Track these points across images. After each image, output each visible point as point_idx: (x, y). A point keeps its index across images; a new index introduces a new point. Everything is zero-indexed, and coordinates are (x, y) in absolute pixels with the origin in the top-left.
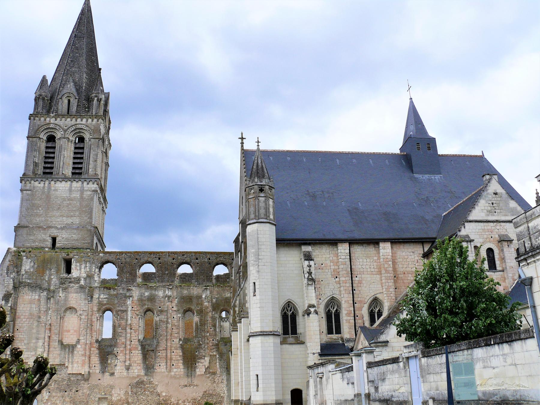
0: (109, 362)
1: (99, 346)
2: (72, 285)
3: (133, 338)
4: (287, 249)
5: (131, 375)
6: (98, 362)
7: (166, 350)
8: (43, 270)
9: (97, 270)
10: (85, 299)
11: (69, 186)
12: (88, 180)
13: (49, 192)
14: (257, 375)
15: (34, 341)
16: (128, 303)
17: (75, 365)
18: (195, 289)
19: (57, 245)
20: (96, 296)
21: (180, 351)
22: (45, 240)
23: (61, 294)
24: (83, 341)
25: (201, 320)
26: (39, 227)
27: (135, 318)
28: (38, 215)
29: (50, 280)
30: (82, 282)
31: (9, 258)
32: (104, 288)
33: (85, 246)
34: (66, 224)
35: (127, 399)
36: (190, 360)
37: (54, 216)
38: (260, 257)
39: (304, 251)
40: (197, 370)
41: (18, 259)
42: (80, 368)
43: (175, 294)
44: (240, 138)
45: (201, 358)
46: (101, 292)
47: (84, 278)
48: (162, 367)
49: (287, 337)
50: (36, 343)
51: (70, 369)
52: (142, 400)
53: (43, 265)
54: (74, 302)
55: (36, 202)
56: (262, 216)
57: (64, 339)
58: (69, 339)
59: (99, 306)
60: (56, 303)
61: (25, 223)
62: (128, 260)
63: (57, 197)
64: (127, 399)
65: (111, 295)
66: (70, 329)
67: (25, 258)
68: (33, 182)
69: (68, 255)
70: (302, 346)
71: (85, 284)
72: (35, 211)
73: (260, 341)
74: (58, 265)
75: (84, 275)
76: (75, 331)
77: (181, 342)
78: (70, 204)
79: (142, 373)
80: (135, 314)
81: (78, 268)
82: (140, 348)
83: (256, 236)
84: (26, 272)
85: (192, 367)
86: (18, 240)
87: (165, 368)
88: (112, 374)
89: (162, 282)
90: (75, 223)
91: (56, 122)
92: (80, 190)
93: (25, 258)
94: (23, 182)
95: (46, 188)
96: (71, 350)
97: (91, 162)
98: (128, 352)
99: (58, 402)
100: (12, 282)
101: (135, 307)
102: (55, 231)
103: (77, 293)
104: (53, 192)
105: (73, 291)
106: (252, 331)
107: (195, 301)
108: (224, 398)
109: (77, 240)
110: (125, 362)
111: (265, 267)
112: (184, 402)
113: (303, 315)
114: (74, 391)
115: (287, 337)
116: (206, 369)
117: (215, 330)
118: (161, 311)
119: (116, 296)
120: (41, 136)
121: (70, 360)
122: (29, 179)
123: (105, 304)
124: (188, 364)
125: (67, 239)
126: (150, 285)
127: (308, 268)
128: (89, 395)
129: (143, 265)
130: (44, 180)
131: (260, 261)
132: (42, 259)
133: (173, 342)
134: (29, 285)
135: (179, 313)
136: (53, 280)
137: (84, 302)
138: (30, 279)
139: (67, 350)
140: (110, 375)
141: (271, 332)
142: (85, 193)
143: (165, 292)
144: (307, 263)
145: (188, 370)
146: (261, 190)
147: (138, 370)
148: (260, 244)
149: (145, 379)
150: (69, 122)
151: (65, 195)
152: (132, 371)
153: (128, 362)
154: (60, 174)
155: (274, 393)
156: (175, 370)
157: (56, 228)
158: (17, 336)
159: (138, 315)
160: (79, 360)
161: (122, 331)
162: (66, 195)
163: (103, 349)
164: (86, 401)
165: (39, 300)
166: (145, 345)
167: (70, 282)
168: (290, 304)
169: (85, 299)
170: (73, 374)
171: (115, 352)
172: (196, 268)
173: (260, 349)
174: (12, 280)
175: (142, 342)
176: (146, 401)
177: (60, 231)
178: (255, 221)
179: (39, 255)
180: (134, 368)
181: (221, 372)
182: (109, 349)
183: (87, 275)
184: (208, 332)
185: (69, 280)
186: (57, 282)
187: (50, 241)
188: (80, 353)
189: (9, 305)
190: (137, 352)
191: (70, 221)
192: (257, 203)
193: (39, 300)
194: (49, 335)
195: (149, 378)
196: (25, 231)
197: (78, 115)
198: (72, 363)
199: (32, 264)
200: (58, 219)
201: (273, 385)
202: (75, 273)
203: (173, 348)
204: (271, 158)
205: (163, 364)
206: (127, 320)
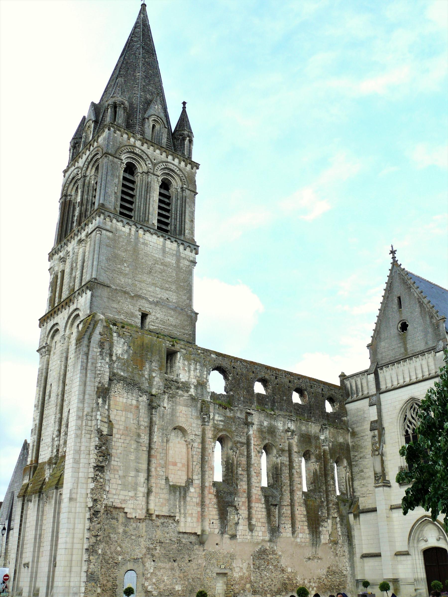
1: (217, 492)
6: (217, 517)
15: (132, 474)
17: (189, 519)
18: (313, 425)
21: (304, 509)
22: (132, 315)
26: (125, 292)
29: (151, 379)
30: (192, 391)
34: (160, 298)
40: (322, 537)
50: (136, 476)
51: (182, 524)
52: (265, 578)
54: (183, 419)
63: (147, 255)
64: (250, 576)
65: (228, 417)
66: (178, 461)
68: (114, 221)
69: (173, 345)
72: (119, 266)
75: (194, 381)
78: (164, 271)
81: (186, 368)
82: (263, 500)
85: (316, 532)
87: (291, 532)
88: (233, 537)
91: (143, 148)
92: (176, 255)
96: (182, 494)
99: (166, 578)
100: (108, 370)
103: (186, 406)
104: (142, 246)
105: (182, 402)
108: (347, 577)
109: (175, 326)
112: (310, 582)
121: (182, 511)
123: (221, 430)
134: (124, 379)
137: (195, 421)
138: (124, 371)
139: (178, 493)
145: (313, 535)
147: (261, 533)
149: (267, 546)
151: (157, 256)
157: (147, 299)
161: (243, 473)
165: (137, 407)
167: (178, 388)
171: (236, 504)
176: (270, 580)
177: (153, 306)
181: (343, 542)
183: (197, 381)
186: (161, 384)
187: (139, 315)
191: (165, 295)
193: (137, 407)
195: (272, 546)
199: (126, 348)
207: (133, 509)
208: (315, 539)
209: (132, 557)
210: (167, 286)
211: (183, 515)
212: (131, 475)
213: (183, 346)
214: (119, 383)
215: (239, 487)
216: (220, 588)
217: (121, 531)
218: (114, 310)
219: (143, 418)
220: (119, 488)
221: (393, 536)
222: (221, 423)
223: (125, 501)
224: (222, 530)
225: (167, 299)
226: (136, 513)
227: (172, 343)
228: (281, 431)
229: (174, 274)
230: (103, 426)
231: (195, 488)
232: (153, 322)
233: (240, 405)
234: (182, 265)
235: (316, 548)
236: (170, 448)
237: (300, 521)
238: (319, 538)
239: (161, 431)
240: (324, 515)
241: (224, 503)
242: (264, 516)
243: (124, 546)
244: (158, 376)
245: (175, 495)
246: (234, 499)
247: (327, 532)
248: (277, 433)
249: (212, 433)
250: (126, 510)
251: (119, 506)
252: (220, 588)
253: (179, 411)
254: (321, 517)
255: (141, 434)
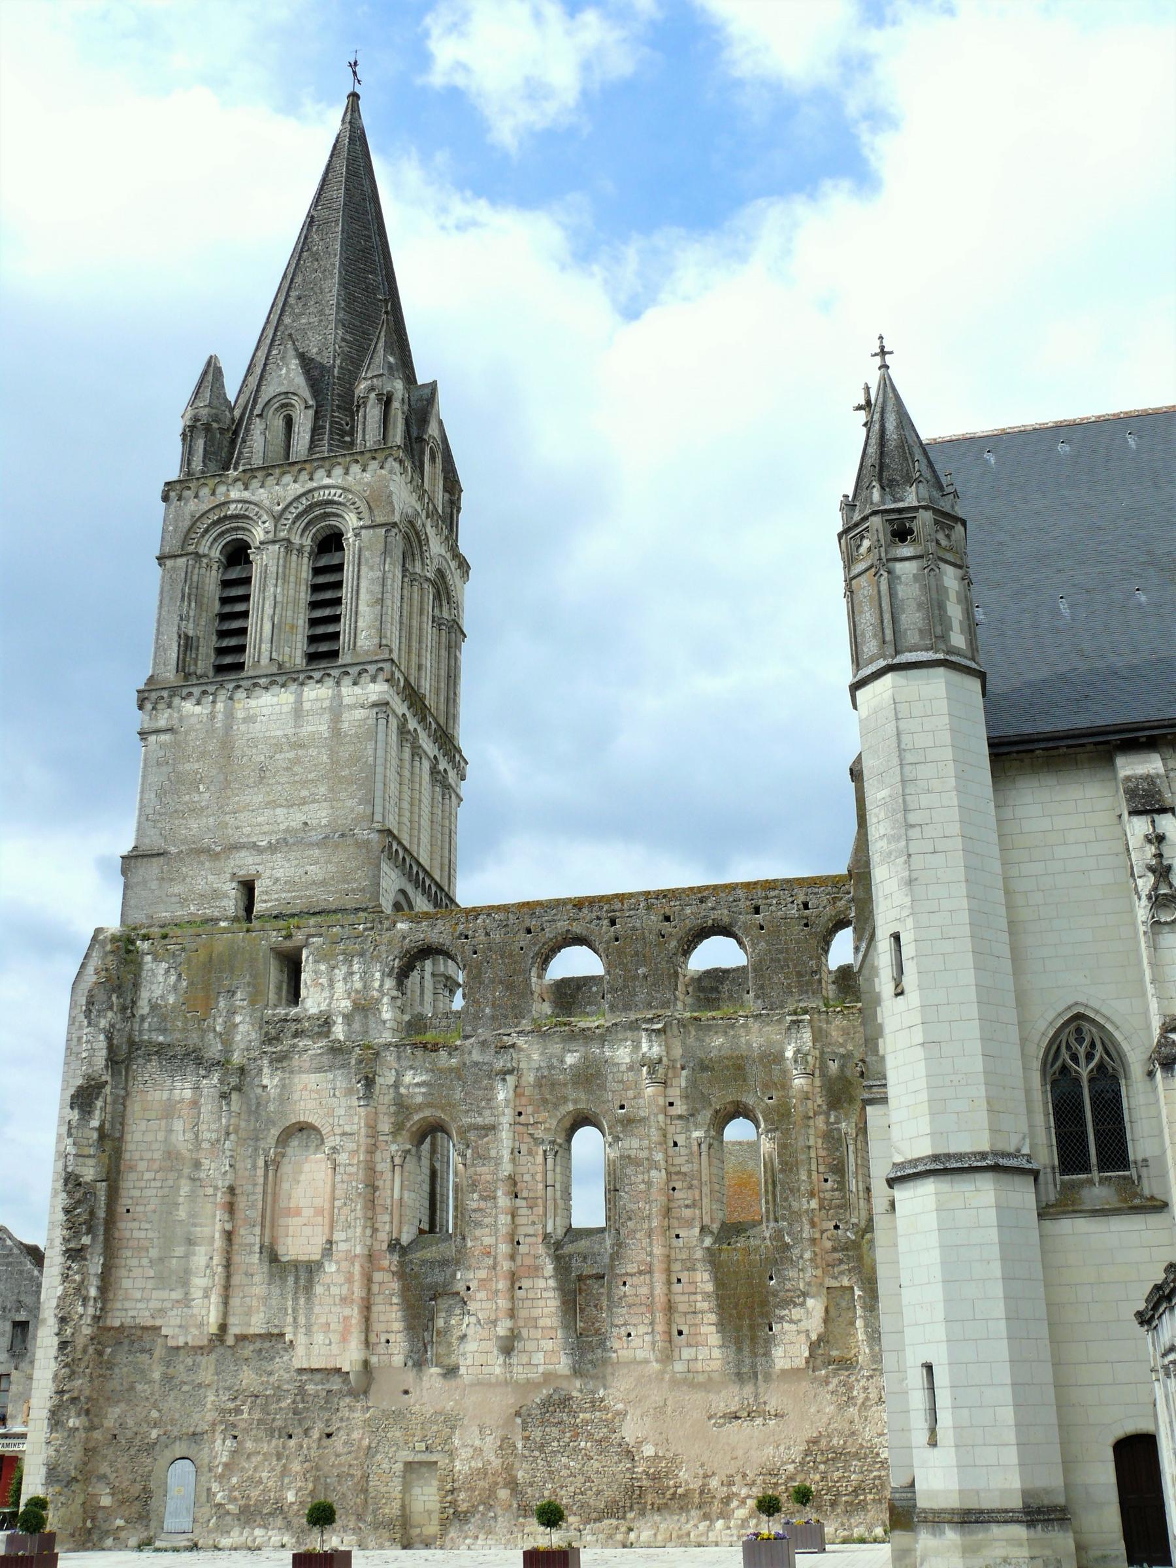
0: (440, 1323)
1: (402, 1264)
2: (302, 1043)
3: (522, 1230)
4: (1050, 780)
5: (520, 1374)
7: (650, 1272)
8: (208, 997)
9: (389, 983)
10: (349, 1092)
11: (292, 698)
12: (354, 671)
13: (228, 728)
14: (929, 1368)
16: (501, 1096)
17: (319, 1338)
19: (258, 907)
20: (386, 1078)
21: (706, 1276)
22: (216, 895)
23: (270, 1080)
24: (343, 1246)
25: (783, 1147)
27: (530, 1153)
28: (197, 811)
29: (231, 1028)
30: (339, 1031)
31: (95, 961)
32: (415, 1046)
33: (350, 902)
34: (287, 830)
35: (509, 1468)
36: (747, 1313)
37: (246, 808)
38: (913, 818)
39: (1128, 779)
40: (778, 1352)
41: (125, 963)
42: (335, 1349)
43: (678, 1052)
44: (859, 408)
45: (789, 1303)
46: (405, 1063)
47: (345, 1016)
48: (636, 1342)
49: (1082, 1183)
50: (187, 1256)
51: (300, 1350)
52: (564, 1472)
53: (208, 979)
54: (311, 1105)
55: (188, 766)
56: (913, 637)
57: (281, 1240)
58: (300, 1242)
59: (396, 1114)
60: (250, 1112)
61: (154, 841)
62: (497, 936)
63: (253, 742)
64: (509, 1468)
65: (441, 1071)
67: (148, 958)
69: (289, 937)
70: (1153, 1220)
71: (348, 1038)
73: (931, 1203)
74: (254, 976)
75: (345, 1005)
76: (319, 1212)
77: (708, 1241)
78: (297, 761)
79: (563, 1364)
80: (527, 1139)
82: (549, 1268)
83: (890, 729)
84: (154, 1007)
85: (753, 1339)
86: (132, 902)
87: (647, 1346)
88: (451, 1372)
89: (627, 1008)
90: (314, 822)
91: (246, 495)
92: (331, 708)
93: (148, 958)
94: (149, 706)
95: (220, 716)
96: (302, 1282)
97: (363, 608)
98: (502, 1285)
99: (265, 1475)
100: (104, 1044)
101: (530, 1109)
102: (250, 860)
103: (320, 1070)
104: (243, 728)
106: (899, 1159)
107: (756, 1074)
109: (323, 883)
110: (494, 1323)
111: (939, 859)
112: (731, 1484)
113: (1151, 1074)
114: (315, 1434)
115: (1082, 1183)
116: (813, 1347)
117: (842, 1186)
118: (628, 1122)
119: (457, 1073)
120: (203, 549)
121: (302, 1320)
122: (165, 694)
123: (420, 1107)
124: (738, 1329)
125: (291, 883)
126: (582, 1025)
127: (1151, 850)
128: (370, 1452)
129: (559, 949)
130: (211, 689)
131: (915, 833)
132: (201, 959)
133: (675, 1242)
134: (160, 1051)
135: (697, 1126)
136: (241, 1028)
139: (291, 1280)
140: (445, 1376)
141: (983, 1155)
142: (346, 716)
143: (637, 1046)
144: (1139, 827)
145: (739, 1350)
146: (902, 534)
147: (547, 1353)
148: (909, 758)
150: (291, 488)
151: (280, 733)
152: (525, 1360)
153: (509, 1324)
154: (264, 661)
155: (1011, 1455)
156: (687, 1353)
157: (254, 846)
158: (127, 1234)
159: (538, 1142)
160: (333, 1319)
161: (482, 1204)
162: (281, 730)
163: (417, 1276)
164: (359, 1473)
165: (195, 1104)
166: (571, 1256)
167: (297, 1034)
168: (1086, 1026)
169: (349, 1092)
170: (312, 1371)
171: (460, 1287)
172: (753, 945)
173: (934, 1239)
174: (102, 1037)
175: (558, 1245)
176: (581, 1479)
178: (882, 663)
179: (193, 946)
180: (531, 1345)
182: (438, 1277)
184: (812, 1195)
185: (294, 1027)
186: (253, 1036)
187: (231, 890)
188: (335, 1290)
189: (95, 1123)
190: (541, 1283)
191: (296, 818)
192: (884, 587)
193: (195, 1104)
194: (228, 1227)
195: (591, 1386)
196: (153, 868)
197: (313, 461)
198: (309, 1328)
200: (260, 816)
201: (1008, 1414)
202: (313, 1001)
203: (677, 1267)
204: (991, 458)
205: (642, 1329)
206: (498, 1161)
207: (180, 1326)
208: (748, 1361)
209: (184, 1430)
210: (305, 793)
211: (303, 1330)
212: (177, 1254)
213: (313, 931)
214: (150, 1061)
215: (469, 1244)
216: (432, 1498)
217: (156, 1375)
218: (174, 899)
219: (208, 1123)
220: (149, 1286)
221: (951, 1333)
222: (417, 1090)
223: (162, 1311)
224: (416, 1357)
225: (306, 824)
226: (186, 1336)
227: (284, 933)
228: (623, 1068)
229: (325, 757)
230: (84, 1165)
231: (337, 1263)
232: (267, 893)
233: (480, 1031)
234: (346, 725)
235: (755, 1384)
236: (285, 1177)
237: (685, 1314)
238: (767, 1354)
239: (251, 1143)
240: (788, 1286)
241: (422, 1290)
242: (553, 1310)
243: (165, 1406)
244: (248, 1019)
245: (283, 1286)
246: (454, 1276)
247: (803, 1337)
248: (610, 1077)
249: (392, 1120)
250: (164, 1332)
251: (149, 1323)
252: (432, 1498)
253: (300, 1087)
254: (775, 1295)
255: (203, 1160)
